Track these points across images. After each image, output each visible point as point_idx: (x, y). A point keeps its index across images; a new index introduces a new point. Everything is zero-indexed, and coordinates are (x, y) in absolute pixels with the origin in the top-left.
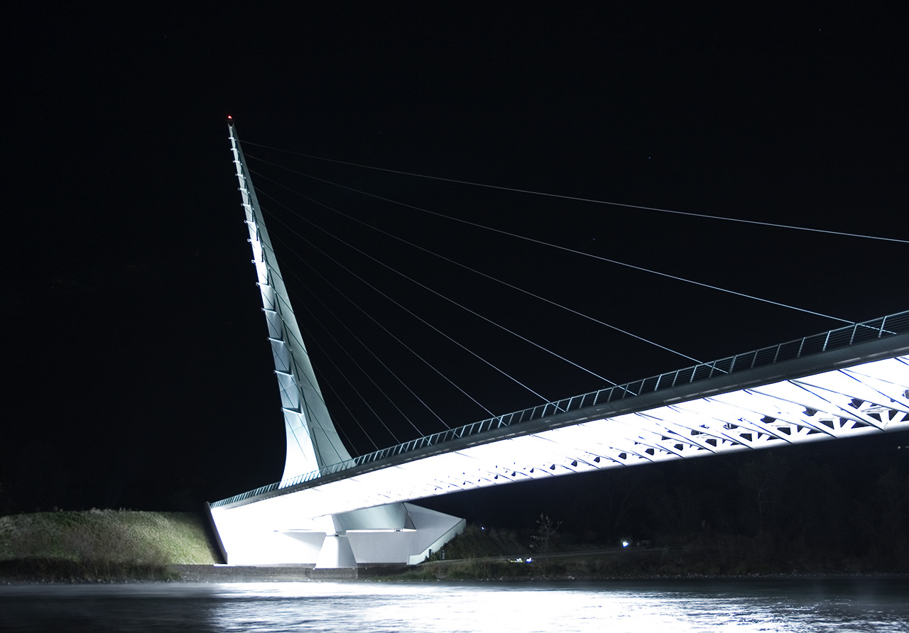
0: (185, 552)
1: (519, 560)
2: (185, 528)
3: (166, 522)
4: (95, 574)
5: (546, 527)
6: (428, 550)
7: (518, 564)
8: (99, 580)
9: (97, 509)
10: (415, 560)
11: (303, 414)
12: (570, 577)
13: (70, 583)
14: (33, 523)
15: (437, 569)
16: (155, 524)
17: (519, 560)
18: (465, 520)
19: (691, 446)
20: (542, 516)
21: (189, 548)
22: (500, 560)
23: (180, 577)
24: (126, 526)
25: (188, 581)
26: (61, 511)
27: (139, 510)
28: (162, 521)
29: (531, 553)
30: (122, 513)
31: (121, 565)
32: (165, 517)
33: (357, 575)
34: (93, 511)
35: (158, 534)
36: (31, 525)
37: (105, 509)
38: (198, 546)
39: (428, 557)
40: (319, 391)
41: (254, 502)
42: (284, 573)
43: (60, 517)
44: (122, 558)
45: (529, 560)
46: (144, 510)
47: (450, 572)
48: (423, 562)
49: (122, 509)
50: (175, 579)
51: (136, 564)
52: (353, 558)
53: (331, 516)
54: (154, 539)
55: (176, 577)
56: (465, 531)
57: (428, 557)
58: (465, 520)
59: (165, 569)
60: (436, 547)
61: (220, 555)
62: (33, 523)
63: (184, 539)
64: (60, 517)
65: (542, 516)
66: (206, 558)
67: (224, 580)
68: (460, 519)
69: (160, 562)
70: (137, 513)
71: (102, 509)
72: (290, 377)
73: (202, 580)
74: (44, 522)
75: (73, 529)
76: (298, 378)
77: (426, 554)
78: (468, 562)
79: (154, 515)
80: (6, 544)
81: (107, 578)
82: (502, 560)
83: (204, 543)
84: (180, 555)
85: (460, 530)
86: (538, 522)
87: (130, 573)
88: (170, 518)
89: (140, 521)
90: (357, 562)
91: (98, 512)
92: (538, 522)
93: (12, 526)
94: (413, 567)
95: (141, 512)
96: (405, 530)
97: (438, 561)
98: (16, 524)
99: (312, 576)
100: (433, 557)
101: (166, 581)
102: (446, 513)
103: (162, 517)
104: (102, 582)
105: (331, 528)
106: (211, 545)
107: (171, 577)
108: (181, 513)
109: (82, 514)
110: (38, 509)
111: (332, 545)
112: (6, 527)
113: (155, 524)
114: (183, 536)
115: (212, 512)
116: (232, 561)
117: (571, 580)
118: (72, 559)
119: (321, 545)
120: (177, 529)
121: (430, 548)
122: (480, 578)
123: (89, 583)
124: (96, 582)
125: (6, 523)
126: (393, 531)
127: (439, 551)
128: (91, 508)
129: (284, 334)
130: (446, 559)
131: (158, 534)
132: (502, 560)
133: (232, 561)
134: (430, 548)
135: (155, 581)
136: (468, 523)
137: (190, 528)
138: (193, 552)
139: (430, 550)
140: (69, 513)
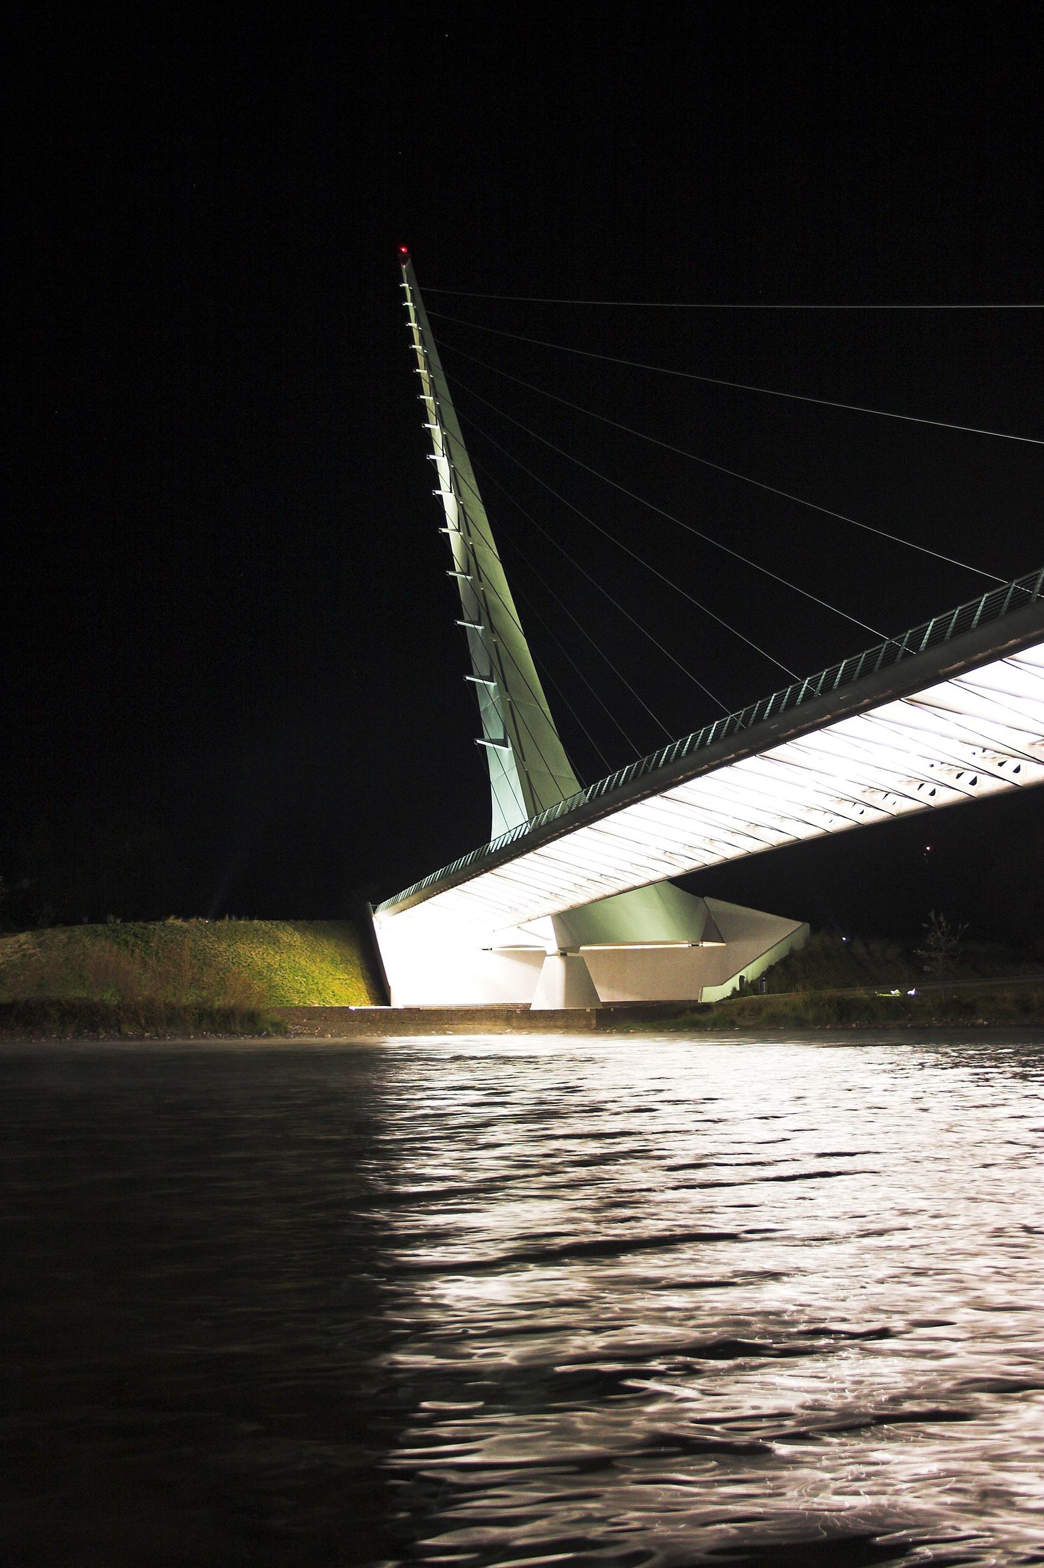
0: (321, 987)
1: (895, 993)
2: (329, 948)
3: (297, 938)
4: (138, 1022)
5: (940, 935)
6: (737, 977)
7: (895, 998)
8: (147, 1034)
9: (177, 918)
10: (713, 994)
11: (510, 749)
12: (980, 1021)
13: (98, 1039)
14: (69, 943)
15: (743, 1009)
16: (276, 941)
17: (895, 993)
18: (807, 925)
19: (855, 803)
20: (932, 915)
21: (330, 979)
22: (858, 993)
23: (285, 1028)
24: (224, 945)
25: (298, 1034)
26: (118, 921)
27: (252, 919)
28: (289, 935)
29: (916, 975)
30: (223, 924)
31: (185, 1008)
32: (295, 929)
33: (594, 1022)
34: (171, 920)
35: (278, 958)
36: (65, 946)
37: (193, 917)
38: (346, 976)
39: (738, 989)
40: (547, 709)
41: (415, 905)
42: (470, 1020)
43: (114, 931)
44: (189, 998)
45: (912, 992)
46: (261, 918)
47: (764, 1014)
48: (728, 998)
49: (230, 918)
50: (276, 1032)
51: (211, 1007)
52: (594, 994)
53: (549, 918)
54: (269, 965)
55: (280, 1029)
56: (808, 943)
57: (738, 989)
58: (807, 925)
59: (259, 1015)
60: (751, 972)
61: (380, 990)
62: (69, 943)
63: (323, 965)
64: (114, 931)
65: (932, 915)
66: (360, 1001)
67: (396, 1032)
68: (799, 924)
69: (253, 1003)
70: (247, 923)
71: (186, 918)
72: (492, 685)
73: (361, 1032)
74: (87, 941)
75: (133, 951)
76: (505, 686)
77: (734, 982)
78: (797, 997)
79: (277, 927)
80: (22, 978)
81: (160, 1031)
82: (860, 993)
83: (357, 971)
84: (311, 992)
85: (799, 943)
86: (925, 925)
87: (200, 1021)
88: (303, 931)
89: (251, 936)
90: (602, 1000)
91: (179, 922)
92: (925, 925)
93: (34, 948)
94: (708, 1006)
95: (256, 921)
96: (706, 944)
97: (754, 996)
98: (40, 945)
99: (515, 1023)
100: (746, 988)
101: (260, 1034)
102: (785, 917)
103: (289, 929)
104: (151, 1038)
105: (548, 938)
106: (368, 975)
107: (270, 1029)
108: (325, 922)
109: (151, 927)
110: (86, 919)
111: (555, 968)
112: (24, 950)
113: (276, 941)
114: (322, 961)
115: (374, 919)
116: (399, 1000)
117: (981, 1026)
118: (102, 1001)
119: (541, 966)
120: (313, 949)
121: (741, 973)
122: (816, 1025)
123: (131, 1039)
124: (141, 1037)
125: (25, 944)
126: (686, 946)
127: (758, 979)
128: (168, 916)
129: (486, 612)
130: (768, 992)
131: (278, 958)
132: (860, 993)
133: (399, 1000)
134: (741, 973)
135: (242, 1034)
136: (815, 929)
137: (337, 946)
138: (336, 986)
139: (742, 978)
140: (130, 925)
